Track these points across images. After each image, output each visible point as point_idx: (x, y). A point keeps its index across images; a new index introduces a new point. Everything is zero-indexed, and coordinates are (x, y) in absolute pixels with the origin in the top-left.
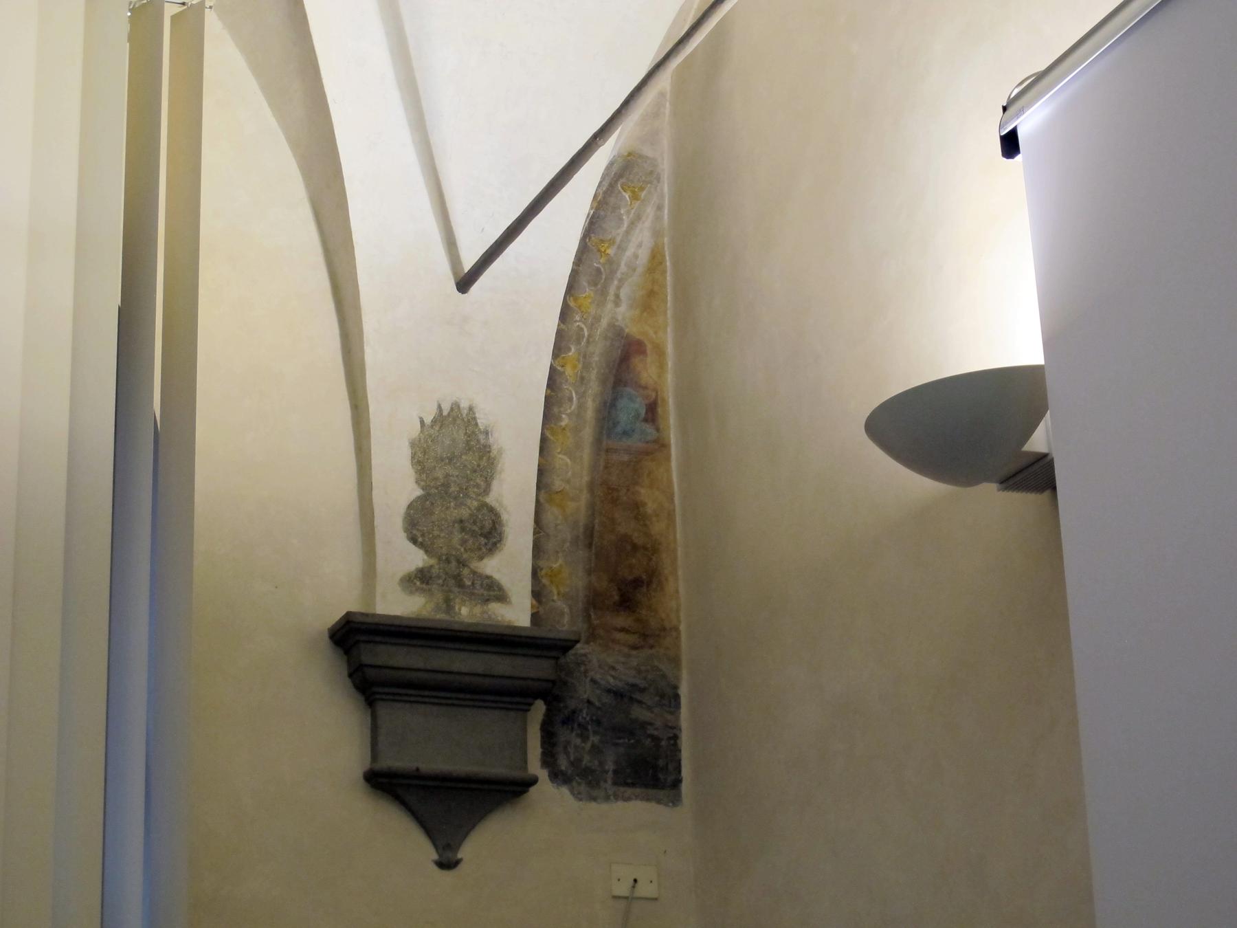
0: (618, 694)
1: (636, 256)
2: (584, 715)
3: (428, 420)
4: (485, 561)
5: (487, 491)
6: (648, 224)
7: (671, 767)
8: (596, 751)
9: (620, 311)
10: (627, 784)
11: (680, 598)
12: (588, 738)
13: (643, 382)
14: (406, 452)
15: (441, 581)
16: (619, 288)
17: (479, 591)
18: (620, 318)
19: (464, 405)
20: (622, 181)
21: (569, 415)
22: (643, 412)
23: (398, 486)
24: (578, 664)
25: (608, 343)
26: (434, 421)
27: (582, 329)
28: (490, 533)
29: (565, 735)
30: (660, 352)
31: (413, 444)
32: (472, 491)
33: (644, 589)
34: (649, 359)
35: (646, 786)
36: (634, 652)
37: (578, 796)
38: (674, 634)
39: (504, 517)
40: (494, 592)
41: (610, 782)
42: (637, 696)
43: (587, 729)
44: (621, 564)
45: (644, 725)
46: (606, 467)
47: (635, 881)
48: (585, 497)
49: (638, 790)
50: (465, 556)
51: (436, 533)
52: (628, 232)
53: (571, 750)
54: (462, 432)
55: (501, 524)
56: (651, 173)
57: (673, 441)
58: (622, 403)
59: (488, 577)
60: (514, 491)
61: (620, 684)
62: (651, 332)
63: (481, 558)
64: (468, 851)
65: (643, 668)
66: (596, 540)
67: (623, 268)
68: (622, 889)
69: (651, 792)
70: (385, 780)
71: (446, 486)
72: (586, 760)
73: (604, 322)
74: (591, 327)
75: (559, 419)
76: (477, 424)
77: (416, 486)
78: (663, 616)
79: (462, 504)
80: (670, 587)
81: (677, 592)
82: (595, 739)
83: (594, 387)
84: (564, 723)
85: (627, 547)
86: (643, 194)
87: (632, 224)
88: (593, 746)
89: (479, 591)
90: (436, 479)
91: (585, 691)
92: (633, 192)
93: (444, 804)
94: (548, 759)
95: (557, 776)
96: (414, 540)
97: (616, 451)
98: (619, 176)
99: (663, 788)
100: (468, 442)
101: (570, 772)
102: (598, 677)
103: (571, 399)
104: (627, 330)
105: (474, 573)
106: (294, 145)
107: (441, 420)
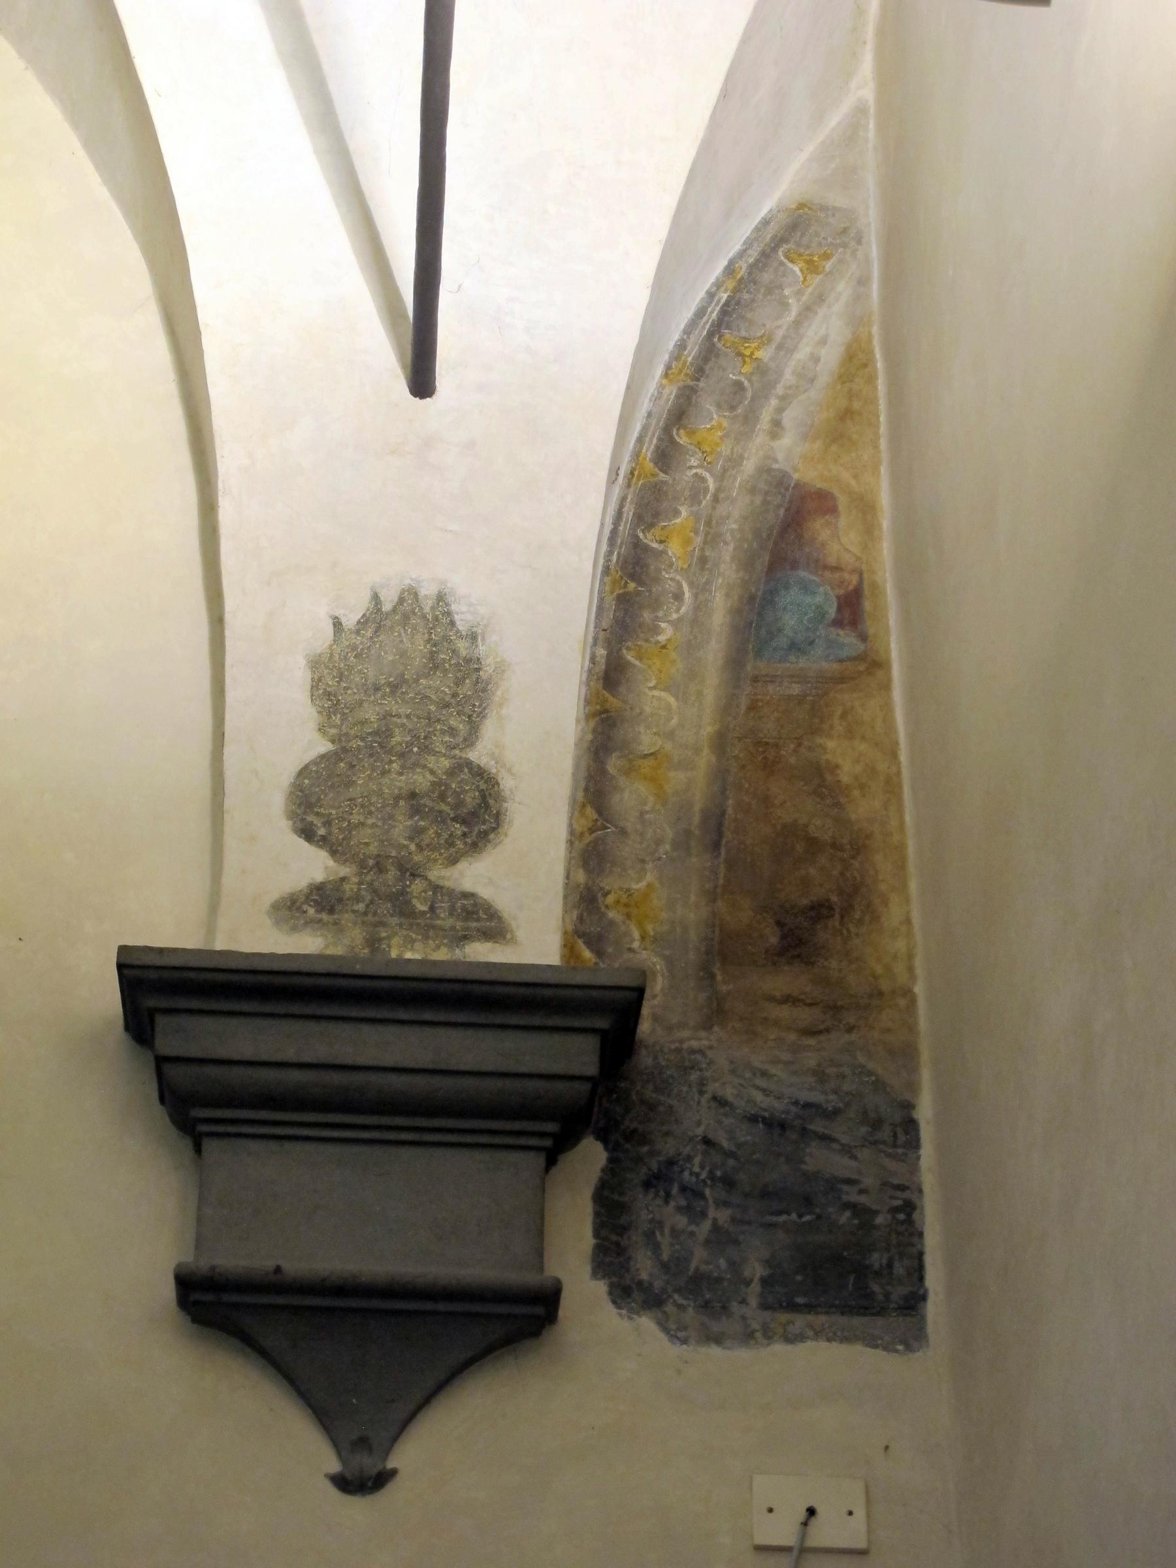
0: (775, 1125)
1: (816, 359)
2: (697, 1167)
3: (350, 620)
4: (462, 865)
5: (471, 739)
6: (838, 308)
7: (899, 1269)
8: (720, 1239)
9: (785, 444)
10: (793, 1307)
11: (912, 930)
12: (704, 1214)
13: (832, 561)
14: (300, 675)
15: (361, 907)
16: (780, 410)
17: (445, 920)
18: (780, 456)
19: (428, 591)
20: (785, 247)
21: (676, 624)
22: (832, 612)
23: (283, 732)
24: (686, 1070)
25: (758, 500)
26: (363, 623)
27: (703, 480)
28: (474, 814)
29: (646, 1208)
30: (866, 507)
31: (315, 664)
32: (439, 743)
33: (835, 922)
34: (843, 521)
35: (847, 1310)
36: (812, 1041)
37: (677, 1334)
38: (902, 1002)
39: (507, 783)
40: (482, 919)
41: (753, 1302)
42: (818, 1126)
43: (702, 1196)
44: (794, 881)
45: (833, 1185)
46: (752, 707)
47: (811, 1512)
48: (706, 759)
49: (821, 1320)
50: (417, 858)
51: (355, 818)
52: (797, 323)
53: (664, 1240)
54: (420, 640)
55: (499, 798)
56: (845, 231)
57: (894, 655)
58: (790, 597)
59: (466, 895)
60: (533, 737)
61: (779, 1106)
62: (846, 476)
63: (453, 861)
64: (408, 1456)
65: (831, 1071)
66: (728, 835)
67: (788, 377)
68: (783, 1531)
69: (857, 1321)
70: (209, 1297)
71: (383, 734)
72: (699, 1258)
73: (749, 466)
74: (721, 477)
75: (656, 630)
76: (452, 623)
77: (317, 736)
78: (879, 970)
79: (416, 765)
80: (893, 915)
81: (908, 921)
82: (723, 1216)
83: (727, 572)
84: (647, 1185)
85: (795, 845)
86: (828, 265)
87: (808, 311)
88: (716, 1228)
89: (445, 920)
90: (364, 723)
91: (697, 1119)
92: (810, 262)
93: (354, 1349)
94: (610, 1258)
95: (627, 1292)
96: (307, 833)
97: (772, 679)
98: (779, 241)
99: (882, 1312)
100: (432, 656)
101: (658, 1284)
102: (729, 1093)
103: (678, 597)
104: (796, 476)
105: (436, 888)
106: (129, 213)
107: (376, 619)
